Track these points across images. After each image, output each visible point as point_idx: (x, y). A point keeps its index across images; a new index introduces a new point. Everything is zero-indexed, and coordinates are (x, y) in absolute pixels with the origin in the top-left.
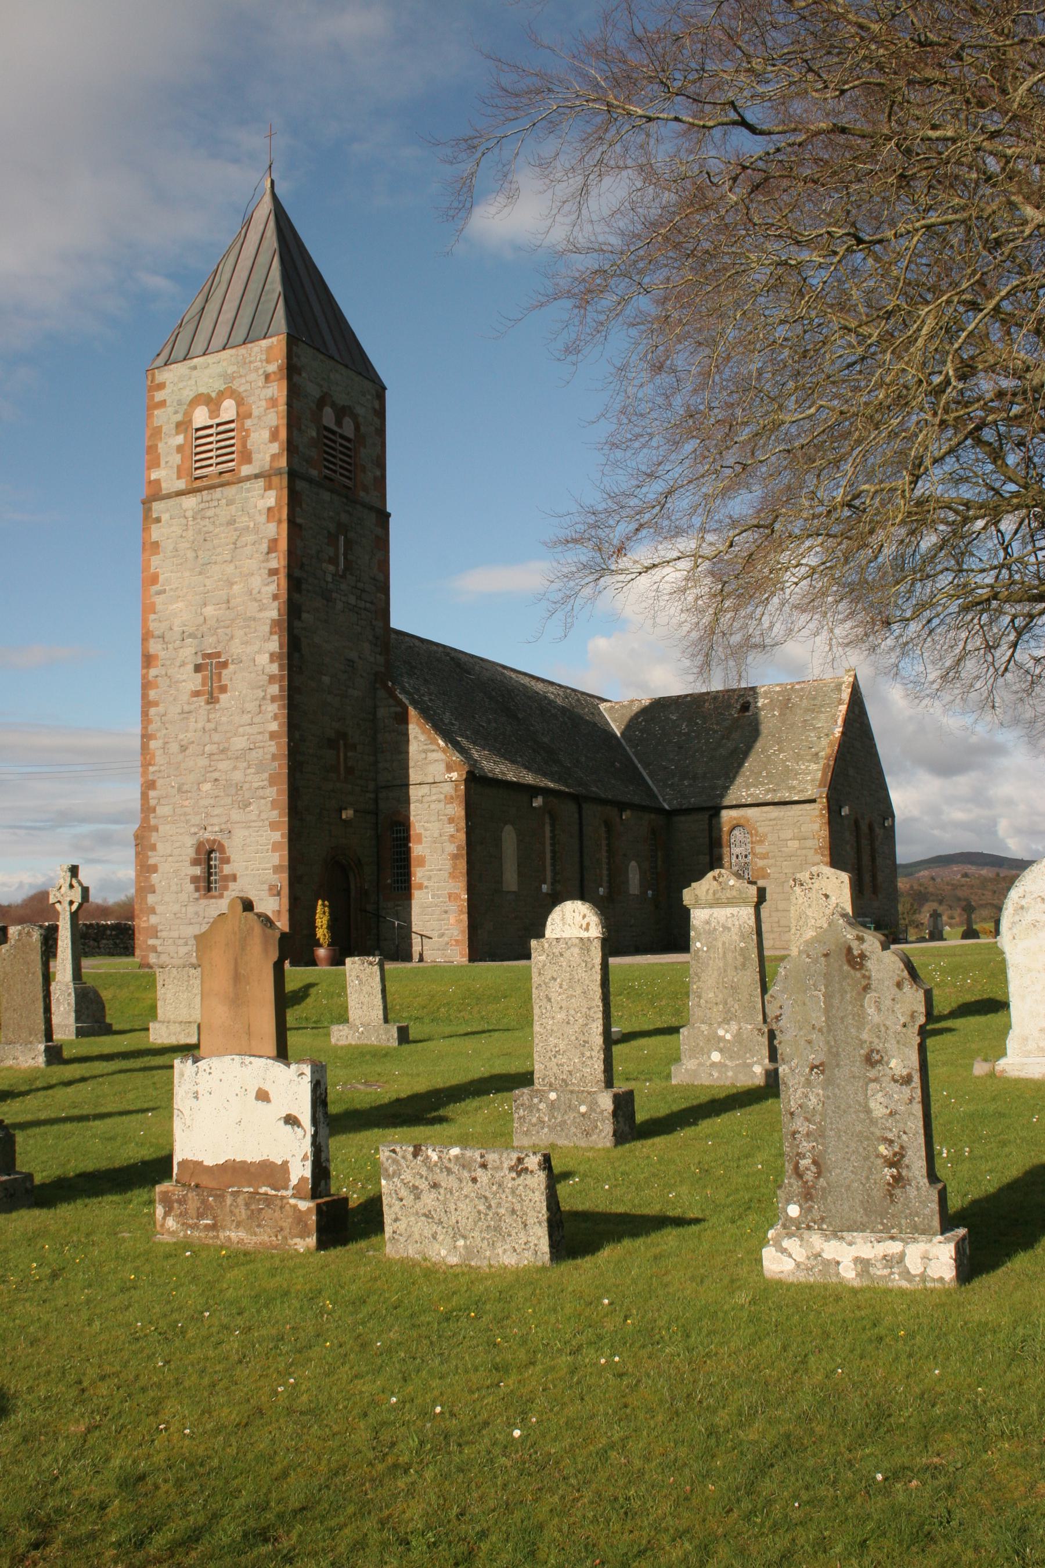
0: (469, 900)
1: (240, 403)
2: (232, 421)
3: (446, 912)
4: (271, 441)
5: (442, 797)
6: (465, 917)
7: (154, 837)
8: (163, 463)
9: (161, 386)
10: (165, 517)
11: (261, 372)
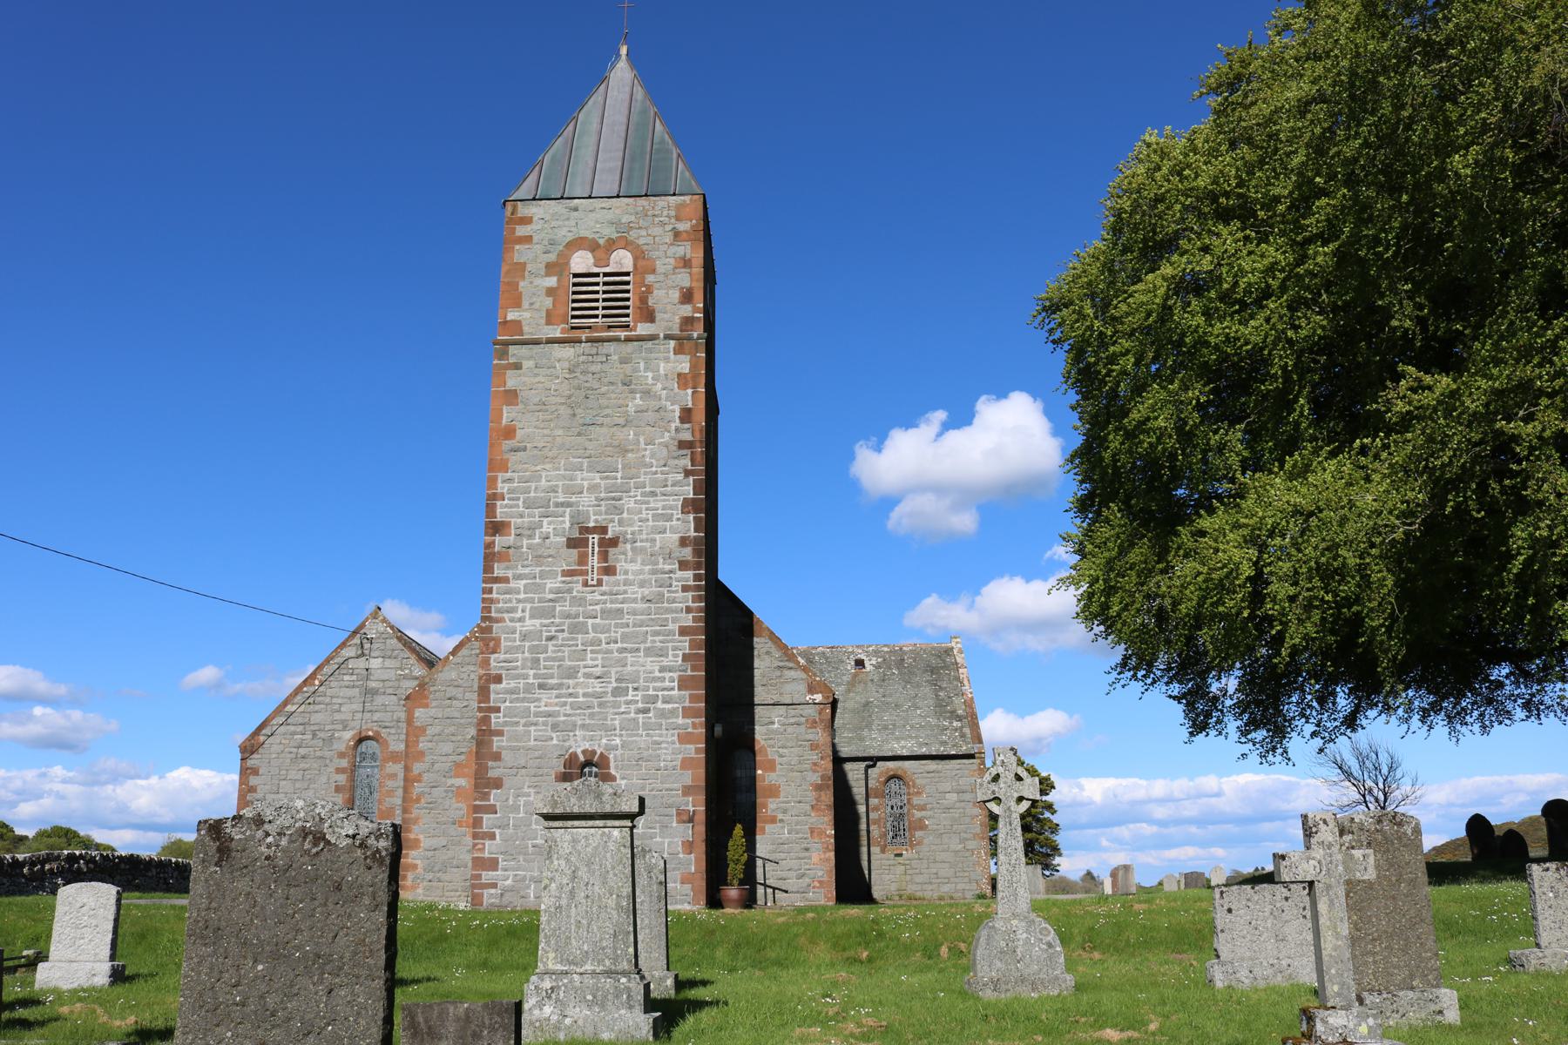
2: (627, 274)
3: (807, 849)
4: (682, 303)
7: (497, 743)
8: (525, 304)
9: (527, 221)
10: (527, 364)
11: (669, 227)
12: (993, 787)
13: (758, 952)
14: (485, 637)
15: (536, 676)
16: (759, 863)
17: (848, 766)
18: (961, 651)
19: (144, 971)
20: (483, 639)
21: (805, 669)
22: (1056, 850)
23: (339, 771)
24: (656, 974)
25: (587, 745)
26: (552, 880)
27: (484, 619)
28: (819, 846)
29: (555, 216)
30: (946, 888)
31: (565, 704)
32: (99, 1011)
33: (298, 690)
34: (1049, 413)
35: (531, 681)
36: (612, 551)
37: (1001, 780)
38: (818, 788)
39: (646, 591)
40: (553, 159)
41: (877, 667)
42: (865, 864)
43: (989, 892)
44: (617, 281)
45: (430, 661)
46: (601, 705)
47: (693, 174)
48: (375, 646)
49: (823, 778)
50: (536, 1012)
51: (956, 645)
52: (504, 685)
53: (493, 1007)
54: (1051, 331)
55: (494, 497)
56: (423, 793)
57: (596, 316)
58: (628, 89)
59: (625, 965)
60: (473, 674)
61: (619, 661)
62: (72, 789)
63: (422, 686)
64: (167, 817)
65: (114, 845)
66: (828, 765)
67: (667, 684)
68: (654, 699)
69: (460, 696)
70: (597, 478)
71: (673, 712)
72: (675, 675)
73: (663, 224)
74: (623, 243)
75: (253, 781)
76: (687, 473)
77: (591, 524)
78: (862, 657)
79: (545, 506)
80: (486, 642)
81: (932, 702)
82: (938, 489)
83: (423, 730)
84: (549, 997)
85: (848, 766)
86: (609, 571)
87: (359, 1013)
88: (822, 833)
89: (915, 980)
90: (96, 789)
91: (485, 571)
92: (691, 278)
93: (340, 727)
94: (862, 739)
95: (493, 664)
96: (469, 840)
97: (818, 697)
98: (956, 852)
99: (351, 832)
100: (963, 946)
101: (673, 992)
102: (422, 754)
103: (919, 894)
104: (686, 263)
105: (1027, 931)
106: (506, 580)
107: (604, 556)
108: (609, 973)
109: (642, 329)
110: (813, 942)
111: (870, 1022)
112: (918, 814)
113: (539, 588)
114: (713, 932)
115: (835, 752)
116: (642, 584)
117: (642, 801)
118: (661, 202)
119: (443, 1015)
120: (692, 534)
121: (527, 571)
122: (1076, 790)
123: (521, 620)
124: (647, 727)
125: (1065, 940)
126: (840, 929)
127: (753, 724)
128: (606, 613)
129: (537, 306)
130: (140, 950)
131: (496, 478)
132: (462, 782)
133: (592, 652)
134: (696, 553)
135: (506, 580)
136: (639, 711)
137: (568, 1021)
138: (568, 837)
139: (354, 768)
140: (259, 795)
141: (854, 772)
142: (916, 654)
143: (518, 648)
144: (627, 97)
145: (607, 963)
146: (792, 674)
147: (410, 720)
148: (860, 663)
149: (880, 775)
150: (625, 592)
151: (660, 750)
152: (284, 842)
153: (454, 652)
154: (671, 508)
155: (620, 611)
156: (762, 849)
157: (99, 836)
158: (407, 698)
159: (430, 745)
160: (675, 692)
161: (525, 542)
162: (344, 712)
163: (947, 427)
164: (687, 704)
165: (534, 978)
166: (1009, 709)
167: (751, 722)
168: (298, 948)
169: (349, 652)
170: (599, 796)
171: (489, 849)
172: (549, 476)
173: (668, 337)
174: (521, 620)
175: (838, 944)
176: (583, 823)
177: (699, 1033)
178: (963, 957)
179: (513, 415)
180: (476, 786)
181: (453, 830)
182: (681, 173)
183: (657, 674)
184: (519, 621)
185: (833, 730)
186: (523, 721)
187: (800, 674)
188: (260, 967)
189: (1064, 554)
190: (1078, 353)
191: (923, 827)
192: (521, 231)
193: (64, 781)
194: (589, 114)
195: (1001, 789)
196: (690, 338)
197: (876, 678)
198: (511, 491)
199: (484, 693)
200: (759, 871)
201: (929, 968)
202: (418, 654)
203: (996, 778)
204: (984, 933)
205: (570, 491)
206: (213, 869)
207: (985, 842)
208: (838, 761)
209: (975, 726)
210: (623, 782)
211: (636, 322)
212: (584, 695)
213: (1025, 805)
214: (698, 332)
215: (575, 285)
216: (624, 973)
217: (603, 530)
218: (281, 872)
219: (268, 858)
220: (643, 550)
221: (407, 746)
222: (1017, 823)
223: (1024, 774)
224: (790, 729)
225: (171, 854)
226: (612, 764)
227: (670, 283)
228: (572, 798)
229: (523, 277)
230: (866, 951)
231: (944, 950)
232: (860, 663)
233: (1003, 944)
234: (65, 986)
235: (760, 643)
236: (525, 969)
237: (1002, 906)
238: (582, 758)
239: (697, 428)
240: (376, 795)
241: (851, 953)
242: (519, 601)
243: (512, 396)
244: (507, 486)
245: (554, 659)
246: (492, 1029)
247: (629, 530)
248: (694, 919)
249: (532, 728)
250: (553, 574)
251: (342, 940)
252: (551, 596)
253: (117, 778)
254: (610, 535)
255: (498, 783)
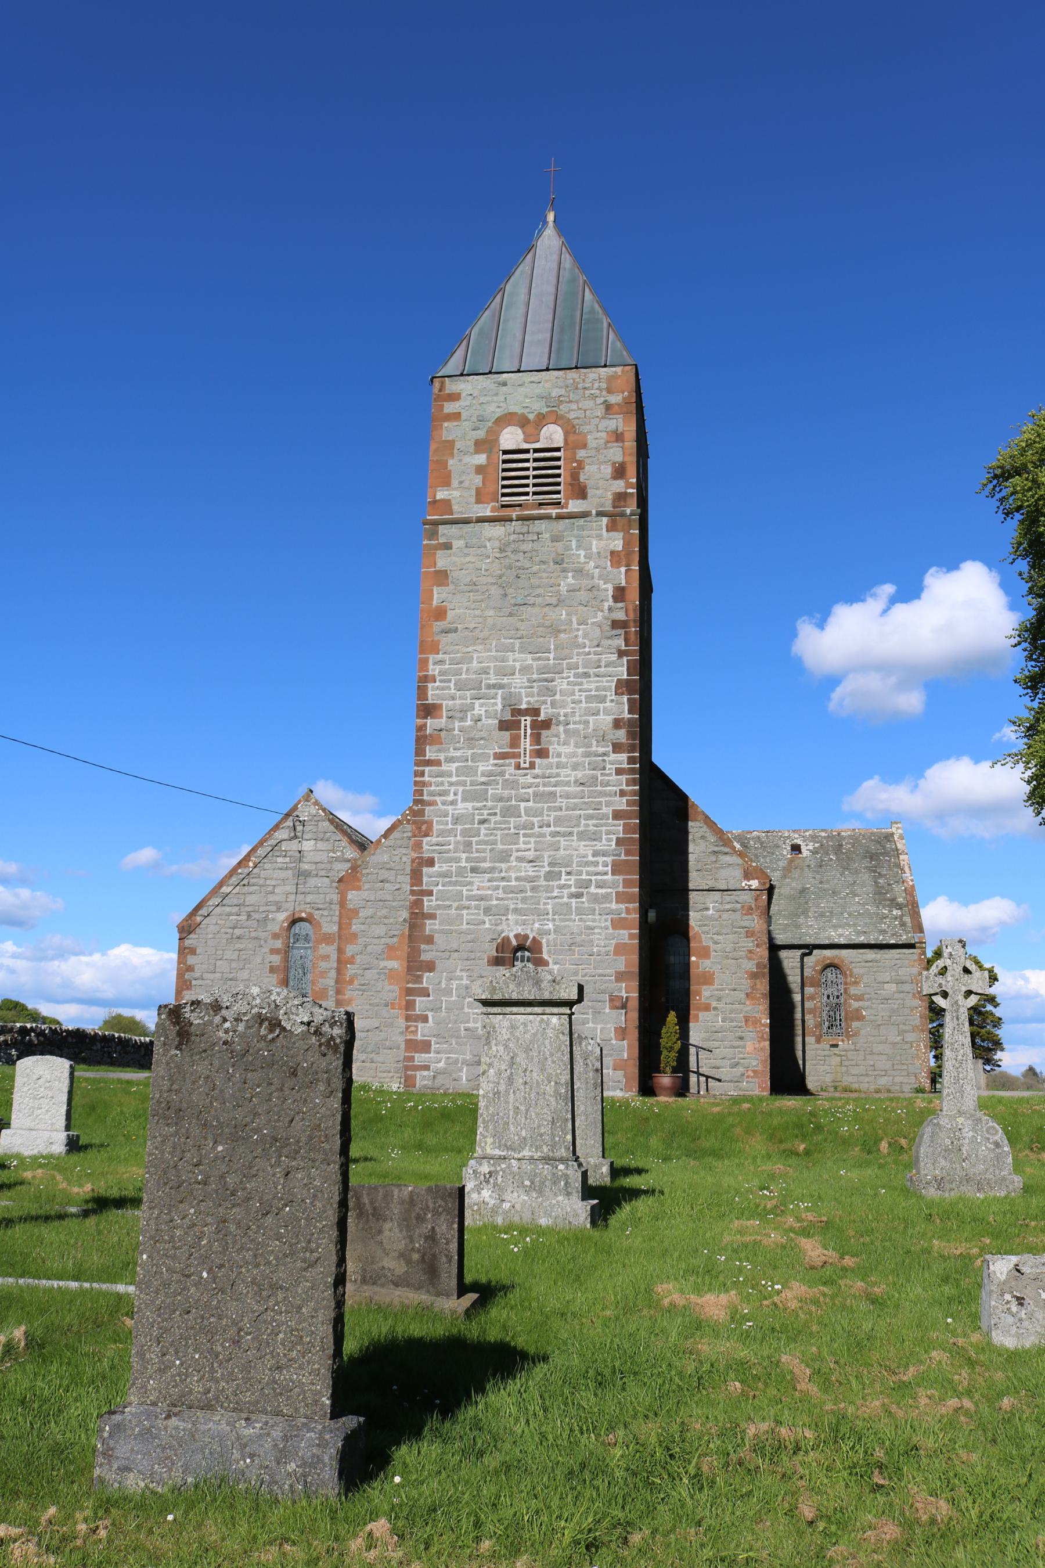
0: (772, 1026)
1: (570, 430)
2: (558, 449)
3: (741, 1038)
5: (739, 906)
6: (767, 1044)
7: (429, 926)
8: (455, 483)
9: (455, 397)
10: (457, 544)
11: (600, 400)
12: (940, 980)
13: (696, 1141)
14: (416, 820)
15: (468, 860)
16: (692, 1051)
17: (783, 954)
18: (901, 837)
19: (96, 1141)
20: (414, 822)
21: (741, 855)
22: (998, 1044)
23: (273, 951)
24: (592, 1161)
25: (519, 930)
26: (490, 1065)
27: (416, 802)
28: (753, 1035)
29: (484, 392)
30: (883, 1081)
31: (497, 888)
32: (59, 1177)
33: (233, 872)
34: (1004, 585)
35: (463, 864)
36: (544, 733)
37: (949, 974)
38: (753, 976)
39: (579, 774)
40: (481, 333)
41: (814, 852)
42: (799, 1054)
43: (927, 1084)
44: (548, 457)
45: (362, 844)
46: (533, 889)
47: (625, 345)
48: (307, 828)
49: (758, 965)
50: (475, 1196)
51: (897, 831)
52: (436, 868)
53: (436, 1192)
54: (1002, 500)
55: (425, 679)
56: (355, 975)
57: (527, 494)
58: (555, 257)
59: (563, 1152)
60: (406, 858)
61: (551, 845)
62: (20, 964)
63: (354, 868)
64: (109, 992)
65: (59, 1018)
66: (764, 953)
67: (600, 868)
68: (587, 884)
69: (392, 879)
70: (529, 660)
71: (606, 897)
72: (609, 859)
73: (594, 397)
74: (553, 418)
75: (191, 960)
76: (621, 654)
77: (524, 706)
78: (799, 842)
79: (477, 689)
80: (418, 825)
81: (871, 889)
82: (883, 667)
83: (356, 912)
84: (487, 1182)
85: (783, 954)
86: (542, 753)
87: (315, 1196)
88: (757, 1022)
89: (855, 1174)
90: (43, 964)
91: (417, 754)
92: (624, 453)
93: (274, 908)
94: (798, 926)
95: (425, 847)
96: (401, 1022)
97: (755, 884)
98: (895, 1044)
99: (306, 1019)
100: (903, 1142)
101: (607, 1180)
102: (355, 936)
103: (855, 1086)
104: (618, 437)
105: (974, 1130)
106: (438, 763)
107: (537, 739)
108: (546, 1159)
109: (574, 506)
110: (748, 1132)
111: (810, 1216)
112: (855, 1004)
113: (471, 771)
114: (647, 1120)
115: (771, 939)
116: (575, 767)
117: (581, 988)
118: (592, 374)
119: (388, 1196)
120: (626, 715)
121: (458, 754)
122: (1021, 982)
123: (453, 803)
124: (580, 911)
125: (1012, 1139)
126: (776, 1121)
127: (688, 910)
128: (538, 797)
129: (466, 484)
130: (90, 1122)
131: (427, 660)
132: (394, 964)
133: (525, 835)
134: (630, 735)
135: (438, 763)
136: (572, 896)
137: (506, 1206)
138: (506, 1024)
139: (287, 950)
140: (197, 974)
141: (790, 960)
142: (855, 839)
143: (450, 831)
144: (555, 265)
145: (545, 1149)
146: (727, 859)
147: (342, 903)
148: (796, 848)
149: (817, 963)
150: (558, 775)
151: (594, 936)
152: (241, 1028)
153: (387, 834)
154: (605, 689)
155: (553, 794)
156: (695, 1036)
157: (46, 1010)
158: (340, 880)
159: (363, 927)
160: (609, 877)
161: (457, 724)
162: (277, 894)
163: (894, 600)
164: (621, 889)
165: (472, 1162)
166: (953, 898)
167: (686, 908)
168: (256, 1131)
169: (282, 834)
170: (537, 983)
171: (422, 1031)
172: (480, 657)
173: (600, 514)
174: (453, 803)
175: (774, 1136)
176: (521, 1009)
177: (636, 1222)
178: (904, 1154)
179: (444, 596)
180: (409, 969)
181: (385, 1012)
182: (612, 343)
183: (590, 858)
184: (451, 803)
185: (770, 917)
186: (455, 905)
187: (735, 859)
188: (220, 1148)
189: (1012, 736)
190: (1031, 520)
191: (860, 1018)
192: (449, 408)
193: (14, 956)
194: (516, 285)
195: (948, 983)
196: (622, 514)
197: (813, 864)
198: (442, 673)
199: (416, 876)
200: (692, 1059)
201: (868, 1164)
202: (349, 837)
203: (944, 971)
204: (928, 1130)
205: (502, 672)
206: (174, 1052)
207: (925, 1036)
208: (774, 949)
209: (916, 915)
210: (556, 967)
211: (567, 499)
212: (517, 879)
213: (973, 1000)
214: (631, 508)
215: (504, 462)
216: (562, 1160)
217: (536, 712)
218: (239, 1055)
219: (225, 1043)
220: (576, 732)
221: (340, 928)
222: (964, 1017)
223: (972, 967)
224: (725, 916)
225: (112, 1028)
226: (545, 949)
227: (602, 458)
228: (507, 982)
229: (452, 455)
230: (806, 1142)
231: (884, 1145)
232: (796, 848)
233: (948, 1142)
234: (27, 1152)
235: (695, 828)
236: (460, 1151)
237: (948, 1102)
238: (514, 943)
239: (631, 607)
240: (309, 976)
241: (787, 1145)
242: (451, 784)
243: (442, 577)
244: (438, 668)
245: (486, 843)
246: (436, 1213)
247: (562, 712)
248: (628, 1106)
249: (465, 912)
250: (484, 757)
251: (298, 1125)
252: (483, 779)
253: (62, 954)
254: (542, 717)
255: (430, 967)
